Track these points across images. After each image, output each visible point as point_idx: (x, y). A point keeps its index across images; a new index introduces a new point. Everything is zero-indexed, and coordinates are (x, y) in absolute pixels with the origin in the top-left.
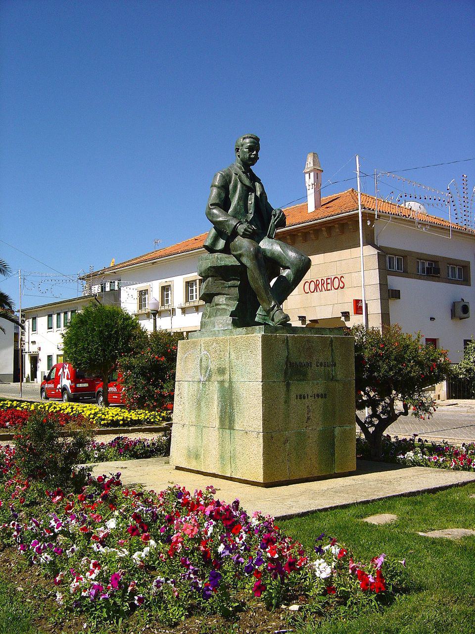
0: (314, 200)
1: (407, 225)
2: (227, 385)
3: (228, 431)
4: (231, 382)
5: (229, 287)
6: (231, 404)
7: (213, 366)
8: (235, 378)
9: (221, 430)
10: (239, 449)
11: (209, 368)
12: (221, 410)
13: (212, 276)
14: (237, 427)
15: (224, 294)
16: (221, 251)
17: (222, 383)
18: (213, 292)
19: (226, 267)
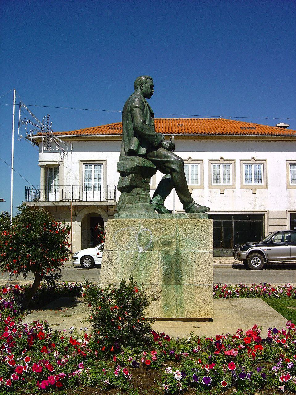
0: (200, 152)
1: (241, 174)
2: (173, 253)
3: (173, 286)
4: (177, 251)
5: (144, 182)
6: (178, 267)
7: (156, 238)
8: (182, 248)
9: (165, 286)
10: (186, 297)
11: (151, 241)
12: (166, 272)
13: (135, 173)
14: (184, 282)
15: (141, 187)
16: (142, 156)
17: (167, 253)
18: (134, 185)
19: (147, 167)
